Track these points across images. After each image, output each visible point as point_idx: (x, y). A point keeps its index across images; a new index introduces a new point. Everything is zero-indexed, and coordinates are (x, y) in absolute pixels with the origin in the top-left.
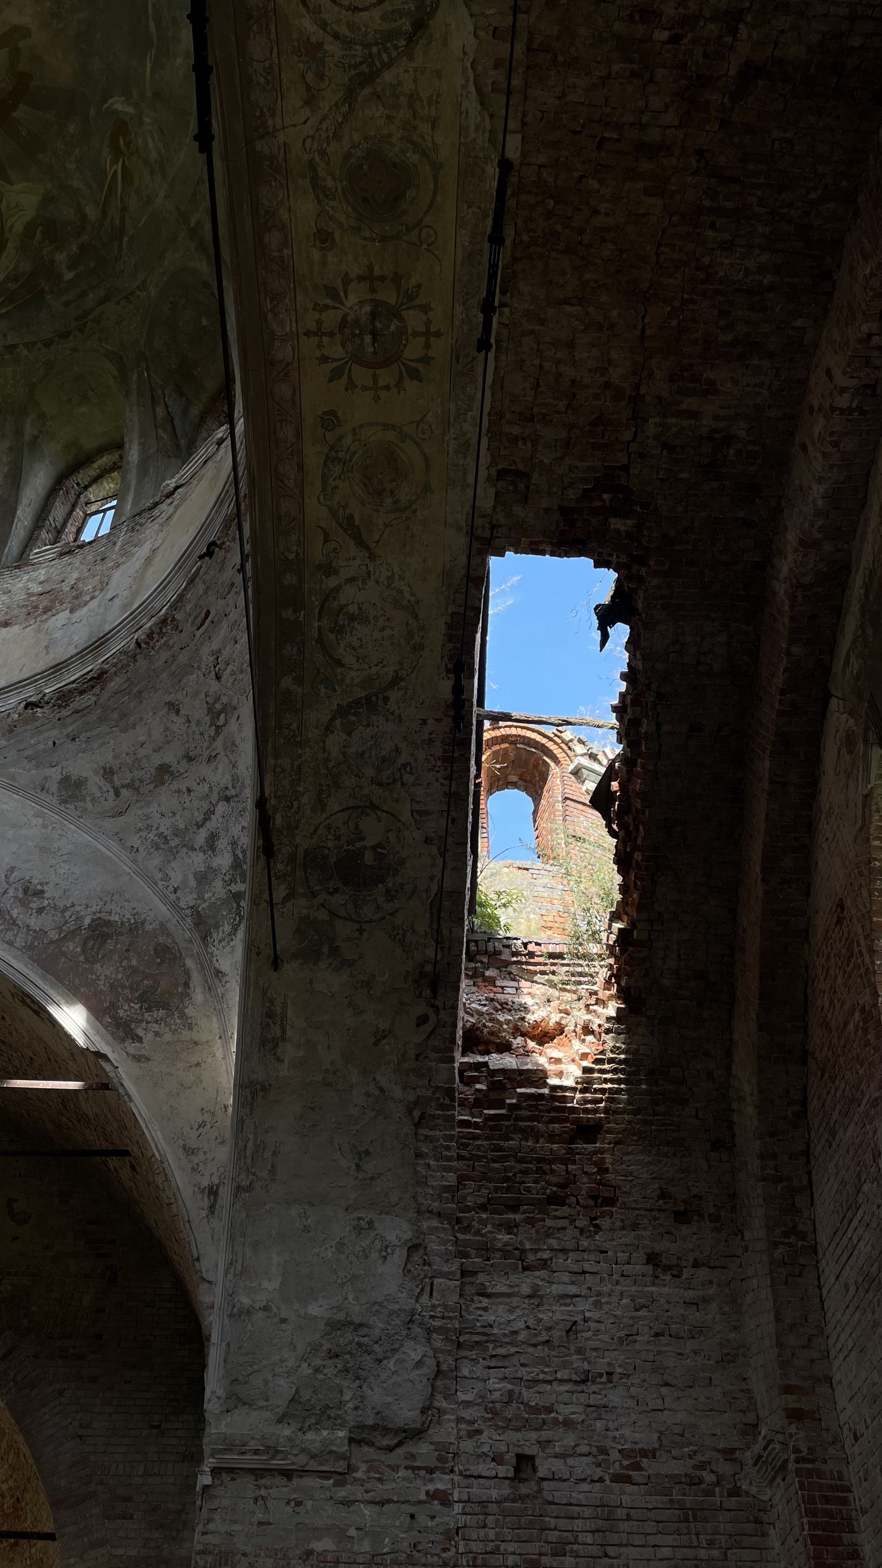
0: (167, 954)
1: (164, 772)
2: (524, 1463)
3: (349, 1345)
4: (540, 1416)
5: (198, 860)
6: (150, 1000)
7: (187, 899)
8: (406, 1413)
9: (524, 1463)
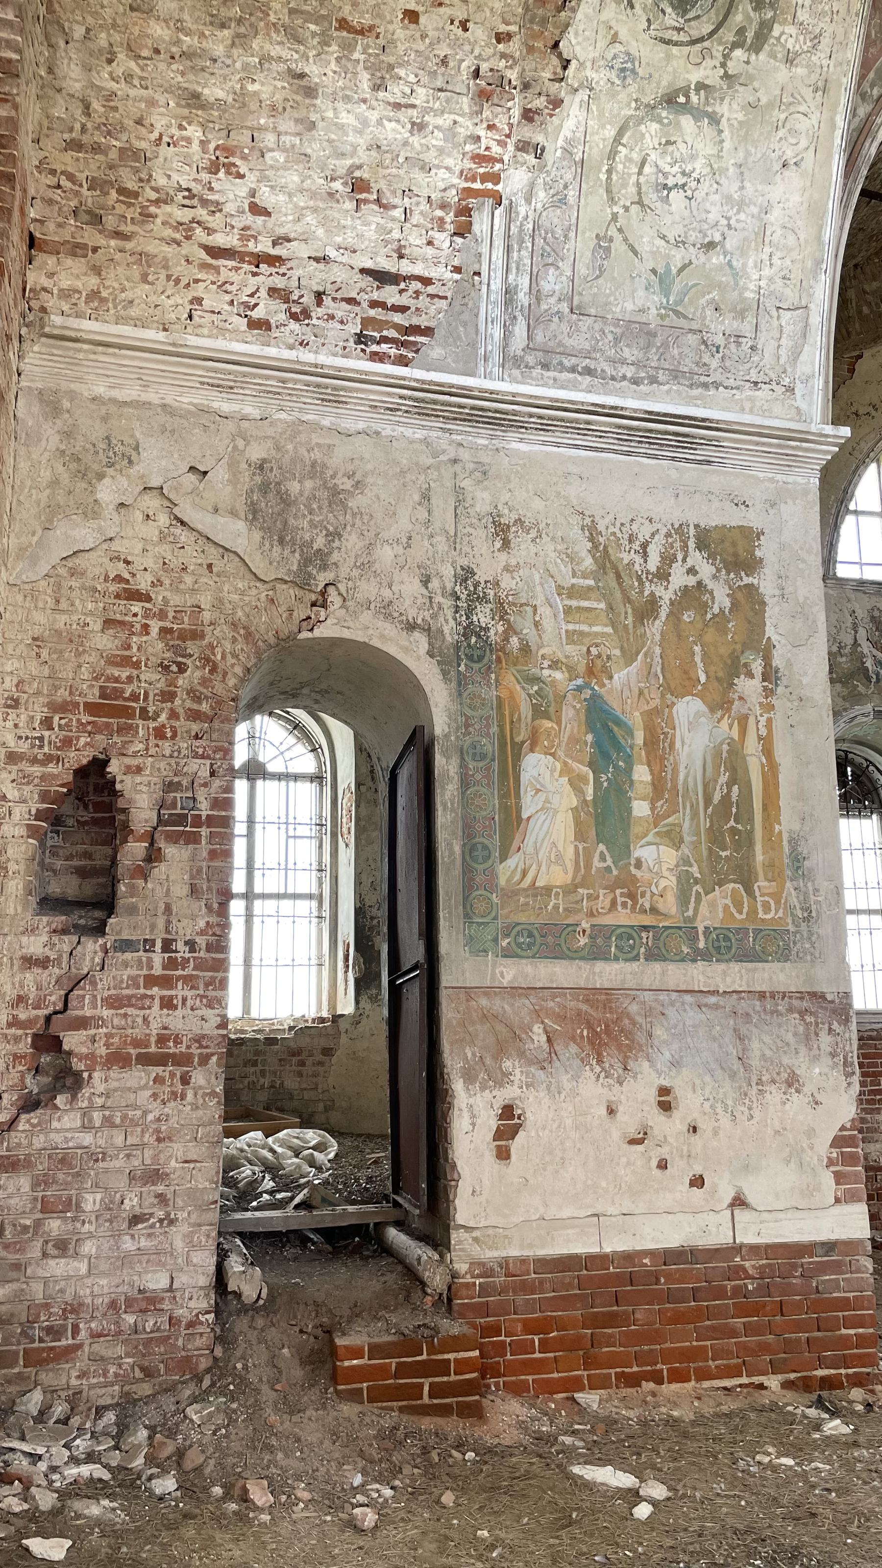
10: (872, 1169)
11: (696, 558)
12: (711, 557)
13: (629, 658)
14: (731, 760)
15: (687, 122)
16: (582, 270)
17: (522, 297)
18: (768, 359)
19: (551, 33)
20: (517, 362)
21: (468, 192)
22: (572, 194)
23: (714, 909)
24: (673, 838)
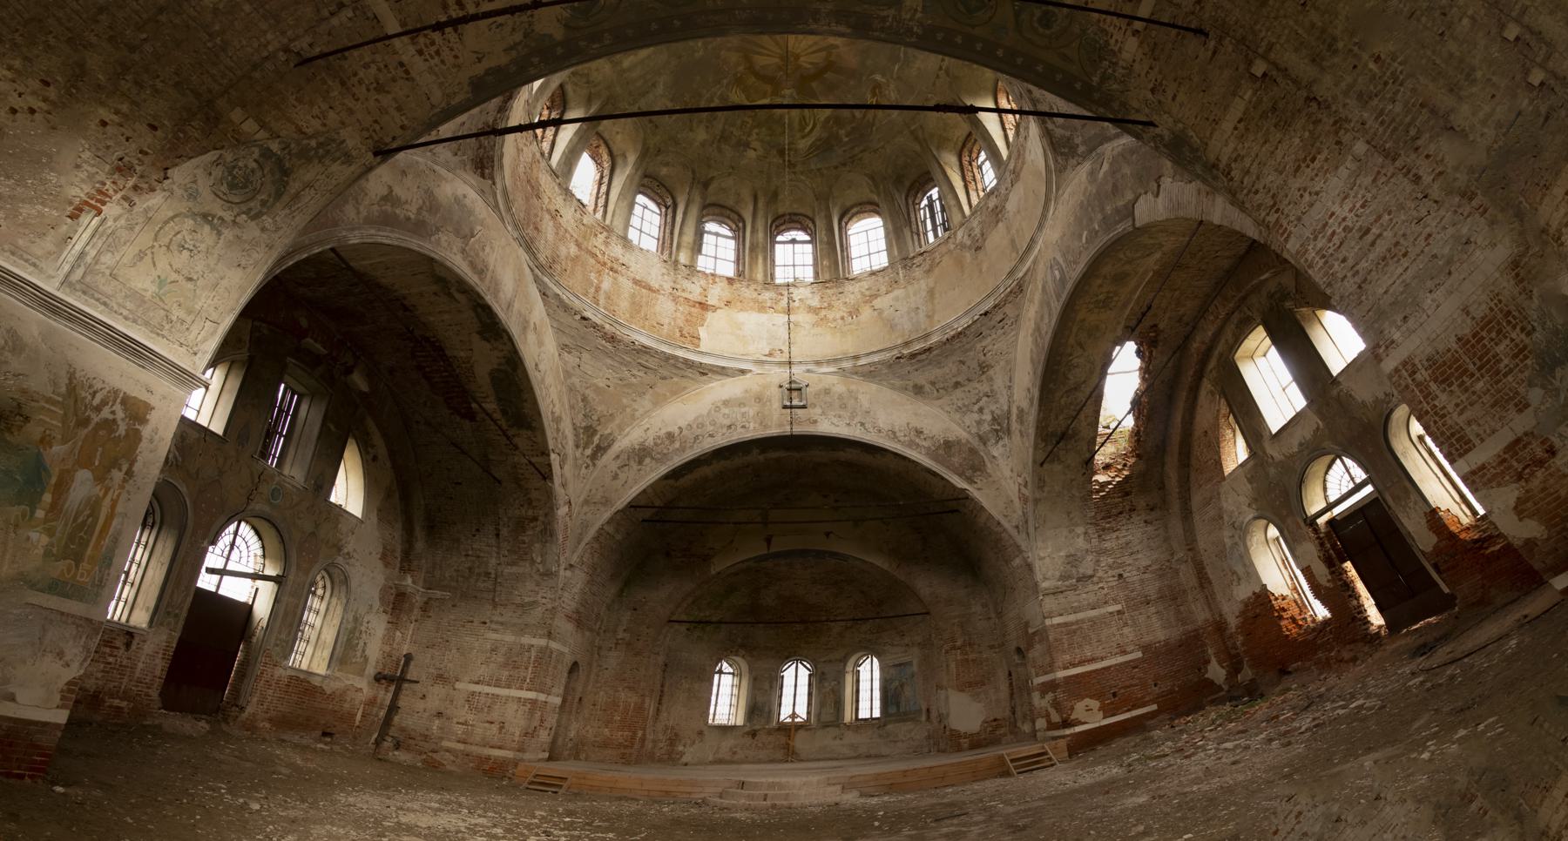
0: (973, 451)
1: (957, 385)
2: (1120, 576)
3: (1073, 560)
4: (1122, 565)
5: (976, 416)
6: (974, 469)
7: (974, 430)
8: (1090, 572)
9: (1120, 576)
10: (33, 481)
11: (118, 407)
12: (125, 410)
13: (64, 441)
14: (93, 505)
15: (207, 228)
16: (125, 260)
17: (89, 259)
18: (192, 337)
19: (168, 163)
20: (71, 285)
21: (86, 203)
22: (137, 228)
23: (59, 568)
24: (50, 532)
